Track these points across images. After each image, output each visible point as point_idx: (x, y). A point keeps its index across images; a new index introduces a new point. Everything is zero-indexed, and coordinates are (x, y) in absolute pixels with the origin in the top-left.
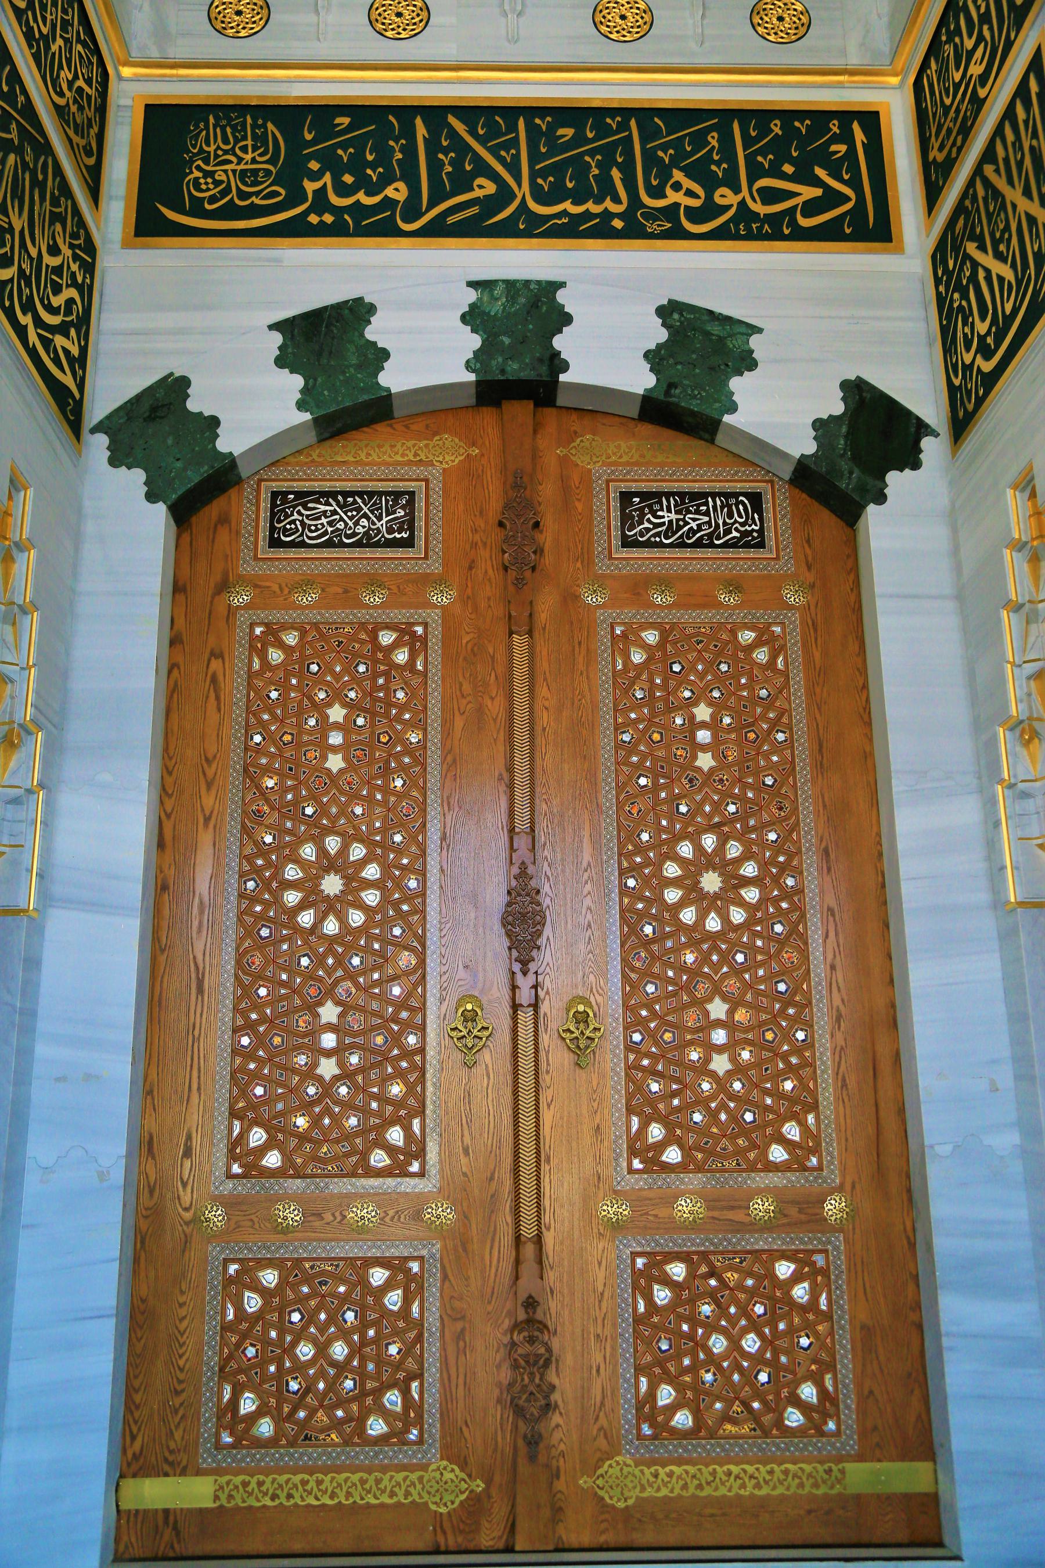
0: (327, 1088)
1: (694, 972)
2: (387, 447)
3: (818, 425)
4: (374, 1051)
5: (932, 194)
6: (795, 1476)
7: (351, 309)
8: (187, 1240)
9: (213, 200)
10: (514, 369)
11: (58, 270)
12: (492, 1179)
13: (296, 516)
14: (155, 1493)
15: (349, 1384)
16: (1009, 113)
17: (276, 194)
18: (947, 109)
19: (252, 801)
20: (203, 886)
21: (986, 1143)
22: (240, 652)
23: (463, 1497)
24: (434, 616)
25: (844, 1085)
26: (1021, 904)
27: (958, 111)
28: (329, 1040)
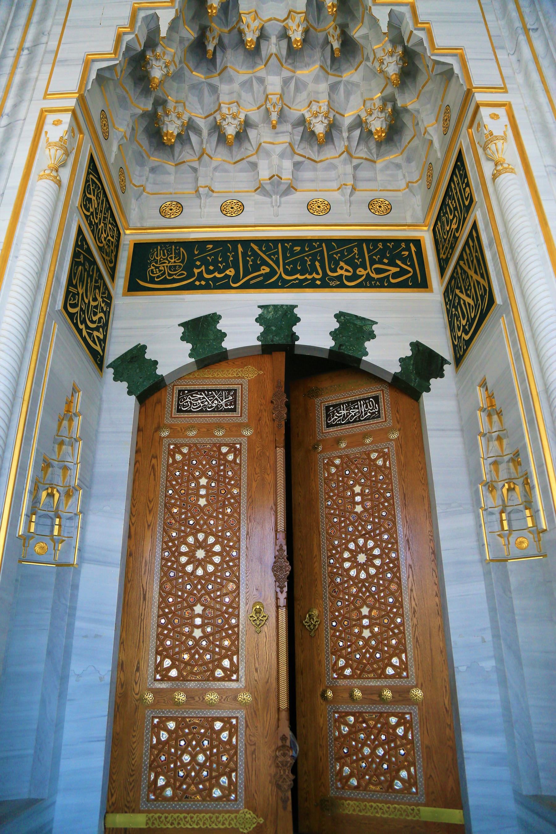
0: (197, 642)
1: (356, 596)
2: (225, 371)
3: (401, 360)
4: (217, 626)
5: (442, 271)
6: (399, 810)
7: (211, 317)
8: (137, 708)
9: (158, 277)
10: (277, 340)
11: (96, 307)
12: (267, 682)
13: (188, 400)
14: (120, 820)
15: (205, 773)
16: (467, 243)
17: (183, 274)
18: (445, 240)
19: (168, 518)
20: (147, 555)
21: (481, 665)
22: (164, 455)
23: (254, 826)
24: (245, 440)
25: (417, 641)
26: (492, 560)
27: (449, 241)
28: (198, 621)
